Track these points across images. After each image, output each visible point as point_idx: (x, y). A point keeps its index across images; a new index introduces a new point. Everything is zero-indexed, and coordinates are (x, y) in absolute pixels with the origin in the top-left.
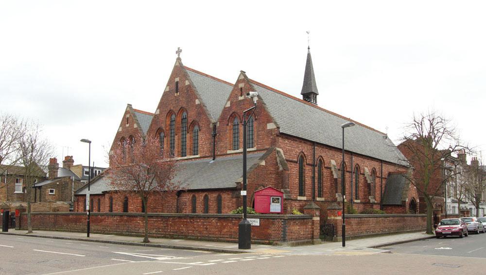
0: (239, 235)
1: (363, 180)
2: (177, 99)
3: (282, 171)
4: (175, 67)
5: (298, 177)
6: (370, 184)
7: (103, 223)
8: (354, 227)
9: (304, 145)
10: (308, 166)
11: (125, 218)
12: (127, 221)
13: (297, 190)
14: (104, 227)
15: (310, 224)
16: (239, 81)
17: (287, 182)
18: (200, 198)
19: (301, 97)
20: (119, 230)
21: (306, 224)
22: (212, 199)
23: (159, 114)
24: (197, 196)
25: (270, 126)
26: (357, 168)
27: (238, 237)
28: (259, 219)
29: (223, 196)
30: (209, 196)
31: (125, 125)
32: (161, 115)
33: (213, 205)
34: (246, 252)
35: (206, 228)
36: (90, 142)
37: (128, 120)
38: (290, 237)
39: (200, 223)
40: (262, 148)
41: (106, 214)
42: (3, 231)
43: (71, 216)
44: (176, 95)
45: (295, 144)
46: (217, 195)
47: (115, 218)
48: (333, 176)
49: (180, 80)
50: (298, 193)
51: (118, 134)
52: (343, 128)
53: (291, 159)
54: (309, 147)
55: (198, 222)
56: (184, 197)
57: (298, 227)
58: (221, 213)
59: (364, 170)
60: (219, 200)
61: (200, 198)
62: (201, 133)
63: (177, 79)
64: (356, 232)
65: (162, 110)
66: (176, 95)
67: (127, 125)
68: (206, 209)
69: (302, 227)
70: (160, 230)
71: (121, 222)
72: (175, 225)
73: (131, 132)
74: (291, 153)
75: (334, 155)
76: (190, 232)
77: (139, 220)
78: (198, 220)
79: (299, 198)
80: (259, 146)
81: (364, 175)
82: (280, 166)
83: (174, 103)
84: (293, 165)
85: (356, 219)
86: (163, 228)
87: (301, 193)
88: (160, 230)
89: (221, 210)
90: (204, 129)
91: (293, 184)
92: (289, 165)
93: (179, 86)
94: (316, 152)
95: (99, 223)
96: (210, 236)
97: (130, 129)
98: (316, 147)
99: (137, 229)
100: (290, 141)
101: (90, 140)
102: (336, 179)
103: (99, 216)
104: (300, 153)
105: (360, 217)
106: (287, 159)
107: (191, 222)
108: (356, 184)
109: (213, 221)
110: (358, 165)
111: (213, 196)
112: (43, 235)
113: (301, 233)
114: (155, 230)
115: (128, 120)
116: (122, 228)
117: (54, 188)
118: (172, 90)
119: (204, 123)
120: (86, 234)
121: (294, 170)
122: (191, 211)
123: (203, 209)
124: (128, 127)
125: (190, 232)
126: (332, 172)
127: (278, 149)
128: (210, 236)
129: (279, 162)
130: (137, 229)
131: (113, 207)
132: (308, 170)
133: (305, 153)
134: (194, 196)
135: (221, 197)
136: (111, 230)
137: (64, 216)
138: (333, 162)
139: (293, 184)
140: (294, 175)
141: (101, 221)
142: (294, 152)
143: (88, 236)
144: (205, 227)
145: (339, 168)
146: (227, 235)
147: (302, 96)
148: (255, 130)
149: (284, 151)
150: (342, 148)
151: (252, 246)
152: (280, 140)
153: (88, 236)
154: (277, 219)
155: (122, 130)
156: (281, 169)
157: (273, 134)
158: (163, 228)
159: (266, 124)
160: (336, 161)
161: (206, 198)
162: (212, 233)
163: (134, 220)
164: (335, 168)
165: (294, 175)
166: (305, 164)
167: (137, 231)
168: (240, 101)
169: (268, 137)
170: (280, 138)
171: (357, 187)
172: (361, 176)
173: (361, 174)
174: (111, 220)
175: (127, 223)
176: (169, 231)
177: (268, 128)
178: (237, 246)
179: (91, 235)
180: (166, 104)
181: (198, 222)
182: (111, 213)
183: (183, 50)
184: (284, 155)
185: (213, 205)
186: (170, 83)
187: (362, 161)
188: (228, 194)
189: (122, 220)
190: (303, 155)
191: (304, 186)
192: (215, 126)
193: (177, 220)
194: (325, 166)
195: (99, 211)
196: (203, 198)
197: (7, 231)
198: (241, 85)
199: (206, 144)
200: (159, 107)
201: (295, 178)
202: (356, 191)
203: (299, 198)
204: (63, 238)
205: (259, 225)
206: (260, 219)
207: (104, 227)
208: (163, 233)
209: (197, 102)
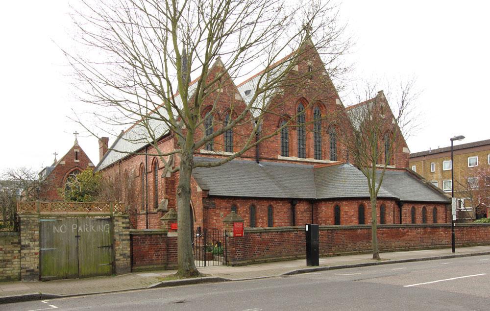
7: (406, 237)
11: (429, 230)
12: (430, 232)
14: (406, 242)
18: (419, 209)
20: (423, 244)
24: (416, 207)
27: (305, 256)
29: (438, 209)
30: (427, 208)
33: (430, 216)
35: (486, 235)
37: (77, 155)
40: (399, 168)
41: (406, 227)
42: (308, 264)
43: (359, 231)
46: (434, 207)
47: (419, 231)
56: (405, 208)
58: (437, 222)
60: (435, 212)
61: (419, 209)
68: (425, 219)
70: (459, 240)
71: (424, 234)
72: (468, 234)
77: (441, 231)
86: (461, 237)
88: (459, 240)
89: (364, 219)
95: (401, 237)
99: (440, 241)
103: (401, 229)
105: (396, 228)
111: (430, 208)
112: (372, 266)
115: (77, 155)
116: (427, 241)
120: (451, 250)
122: (411, 222)
123: (422, 220)
130: (440, 241)
134: (413, 208)
135: (437, 209)
136: (415, 245)
137: (347, 232)
141: (404, 234)
143: (454, 251)
153: (454, 251)
158: (461, 237)
159: (402, 148)
161: (435, 209)
163: (437, 231)
167: (440, 243)
169: (404, 159)
174: (414, 233)
175: (431, 236)
179: (456, 250)
182: (413, 226)
185: (430, 216)
188: (442, 207)
189: (425, 232)
193: (469, 229)
195: (401, 223)
196: (421, 209)
197: (318, 265)
204: (415, 260)
207: (406, 242)
208: (460, 242)
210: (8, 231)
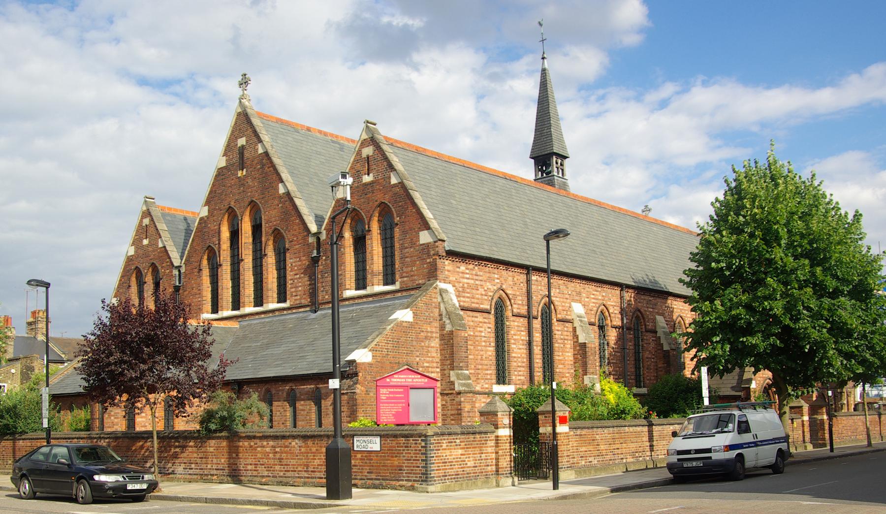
0: (327, 471)
1: (652, 345)
2: (241, 181)
3: (451, 332)
4: (239, 114)
5: (493, 344)
6: (668, 351)
8: (602, 447)
9: (504, 273)
10: (517, 319)
13: (492, 372)
15: (492, 443)
16: (364, 144)
17: (463, 354)
19: (528, 171)
21: (482, 445)
22: (302, 397)
23: (208, 217)
25: (425, 237)
26: (637, 317)
28: (379, 438)
31: (141, 240)
32: (211, 219)
34: (337, 505)
35: (280, 459)
36: (47, 285)
38: (441, 473)
39: (268, 450)
44: (239, 175)
45: (591, 288)
48: (577, 337)
49: (247, 141)
50: (494, 377)
51: (129, 260)
52: (548, 238)
53: (474, 305)
54: (520, 277)
55: (263, 447)
57: (460, 452)
59: (654, 321)
62: (292, 256)
63: (242, 141)
64: (608, 458)
65: (213, 207)
66: (239, 175)
67: (145, 242)
69: (470, 451)
70: (193, 466)
73: (152, 257)
74: (474, 291)
75: (579, 294)
76: (249, 467)
78: (265, 443)
79: (497, 388)
80: (405, 279)
81: (656, 332)
82: (448, 321)
83: (236, 191)
84: (480, 317)
85: (606, 431)
87: (502, 377)
90: (297, 247)
91: (482, 359)
92: (469, 319)
93: (247, 154)
94: (534, 287)
96: (288, 474)
97: (150, 249)
98: (534, 278)
100: (471, 266)
101: (46, 280)
102: (584, 345)
104: (495, 292)
106: (466, 305)
107: (251, 446)
108: (637, 353)
109: (293, 443)
110: (639, 311)
113: (469, 464)
114: (183, 466)
117: (5, 383)
118: (233, 165)
119: (295, 233)
121: (486, 327)
124: (147, 246)
125: (249, 467)
126: (574, 329)
127: (441, 285)
128: (288, 474)
129: (444, 313)
131: (105, 421)
132: (516, 330)
133: (508, 292)
138: (578, 309)
139: (482, 359)
140: (484, 339)
142: (481, 291)
144: (278, 456)
145: (593, 320)
146: (320, 472)
147: (533, 161)
148: (397, 245)
149: (457, 290)
150: (546, 267)
151: (354, 490)
152: (447, 265)
154: (412, 436)
155: (136, 252)
156: (448, 328)
157: (432, 253)
160: (584, 305)
162: (290, 468)
164: (581, 321)
165: (484, 339)
166: (511, 314)
168: (366, 184)
170: (447, 262)
171: (637, 360)
172: (649, 337)
173: (647, 331)
176: (209, 466)
177: (421, 242)
178: (323, 492)
180: (221, 194)
181: (263, 447)
183: (238, 86)
184: (458, 296)
186: (229, 149)
187: (648, 302)
190: (504, 295)
191: (509, 361)
192: (318, 239)
194: (559, 316)
198: (368, 151)
199: (299, 278)
200: (208, 202)
201: (485, 346)
202: (637, 368)
203: (497, 388)
205: (379, 449)
206: (381, 438)
209: (282, 190)
210: (519, 357)
